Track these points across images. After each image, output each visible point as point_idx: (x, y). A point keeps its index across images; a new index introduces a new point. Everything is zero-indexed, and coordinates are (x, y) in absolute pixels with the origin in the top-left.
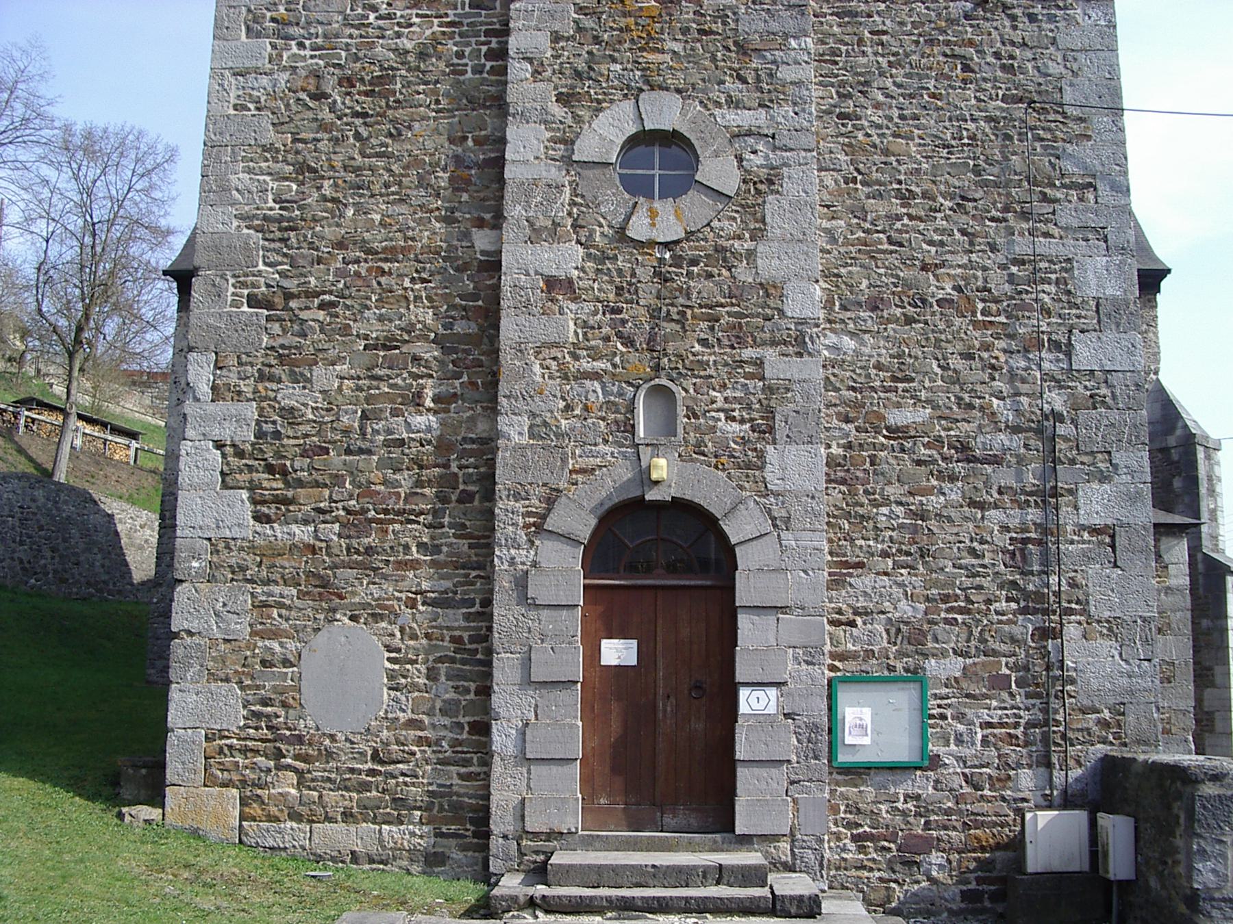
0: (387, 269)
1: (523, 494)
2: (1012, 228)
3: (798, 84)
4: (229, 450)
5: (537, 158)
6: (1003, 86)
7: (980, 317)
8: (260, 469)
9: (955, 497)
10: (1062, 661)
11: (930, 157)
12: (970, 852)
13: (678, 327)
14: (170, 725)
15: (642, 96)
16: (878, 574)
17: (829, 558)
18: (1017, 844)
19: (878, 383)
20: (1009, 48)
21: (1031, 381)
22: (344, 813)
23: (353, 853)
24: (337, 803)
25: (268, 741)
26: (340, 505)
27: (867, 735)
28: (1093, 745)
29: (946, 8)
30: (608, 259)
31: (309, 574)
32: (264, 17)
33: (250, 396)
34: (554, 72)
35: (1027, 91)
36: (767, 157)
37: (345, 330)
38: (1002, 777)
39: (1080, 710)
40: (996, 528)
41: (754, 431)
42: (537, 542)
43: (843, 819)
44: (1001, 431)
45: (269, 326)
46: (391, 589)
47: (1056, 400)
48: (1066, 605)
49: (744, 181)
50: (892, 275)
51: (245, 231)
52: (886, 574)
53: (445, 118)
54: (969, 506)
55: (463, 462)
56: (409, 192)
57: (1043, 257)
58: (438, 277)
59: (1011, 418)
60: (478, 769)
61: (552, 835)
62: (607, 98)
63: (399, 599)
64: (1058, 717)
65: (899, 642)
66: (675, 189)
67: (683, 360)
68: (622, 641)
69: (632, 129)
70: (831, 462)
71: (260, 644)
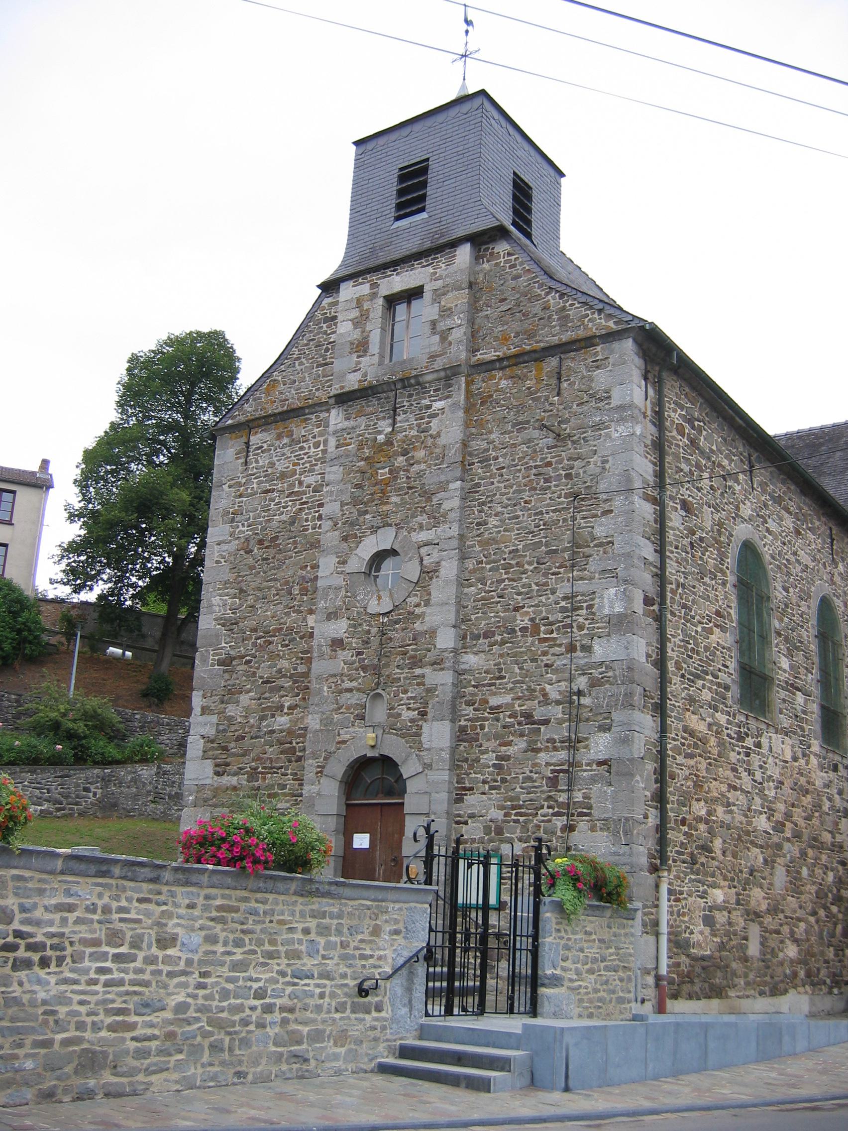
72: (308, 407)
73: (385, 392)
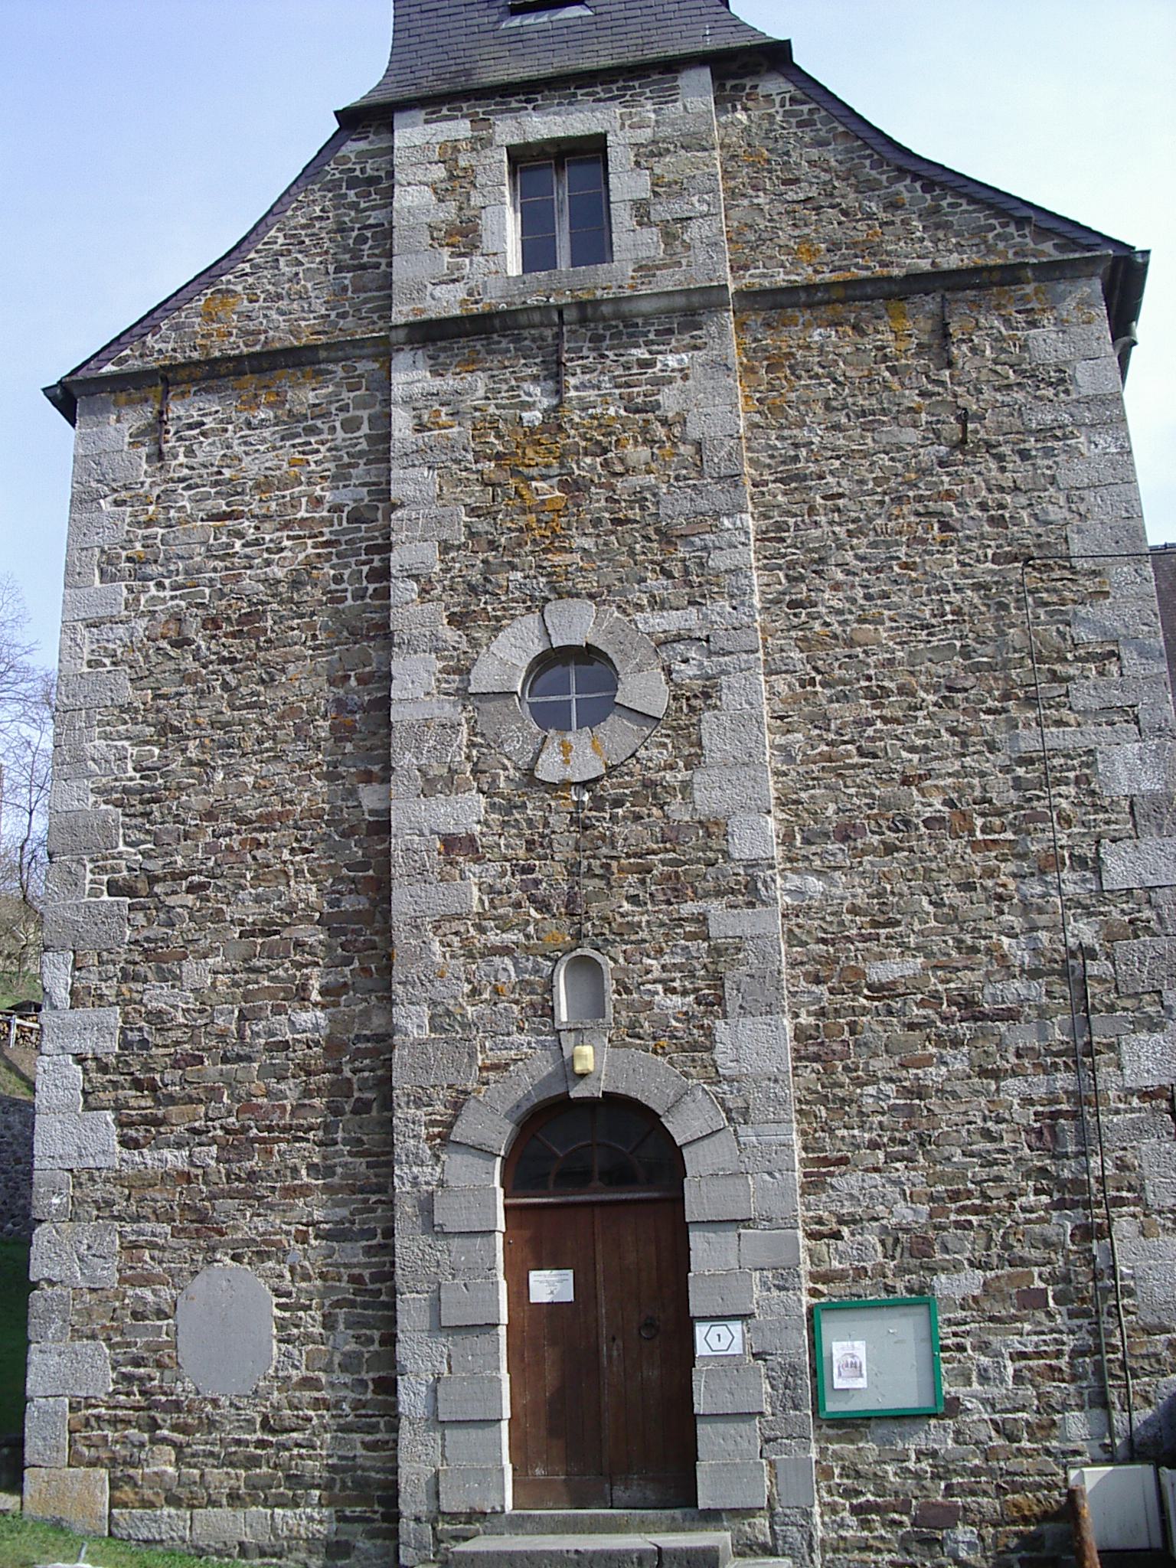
0: (262, 841)
1: (425, 1099)
2: (1015, 719)
3: (735, 571)
4: (90, 1064)
5: (428, 694)
6: (992, 543)
7: (979, 836)
8: (127, 1085)
9: (960, 1066)
10: (1113, 1267)
11: (905, 643)
12: (1008, 1524)
13: (602, 884)
14: (29, 1393)
15: (548, 606)
16: (866, 1170)
17: (804, 1155)
18: (1070, 1509)
19: (854, 932)
20: (997, 495)
21: (1051, 910)
22: (229, 1496)
23: (241, 1544)
24: (221, 1482)
25: (140, 1409)
26: (217, 1124)
27: (861, 1376)
28: (1164, 1375)
29: (915, 456)
30: (516, 807)
31: (184, 1207)
32: (119, 557)
33: (112, 999)
34: (444, 590)
35: (1023, 545)
36: (701, 665)
37: (218, 916)
38: (1045, 1423)
39: (1143, 1330)
40: (1016, 1101)
41: (699, 1004)
42: (444, 1157)
43: (839, 1485)
44: (1014, 977)
45: (132, 916)
46: (278, 1221)
47: (1085, 932)
48: (1115, 1194)
49: (675, 698)
50: (865, 795)
51: (103, 807)
52: (876, 1170)
53: (324, 656)
54: (979, 1076)
55: (357, 1064)
56: (285, 746)
57: (1056, 752)
58: (321, 846)
59: (1027, 960)
60: (386, 1437)
61: (474, 1516)
62: (507, 614)
63: (288, 1233)
64: (1113, 1341)
65: (897, 1255)
66: (594, 715)
67: (610, 924)
68: (555, 1272)
69: (537, 648)
70: (800, 1034)
71: (130, 1292)
72: (327, 346)
73: (533, 326)
